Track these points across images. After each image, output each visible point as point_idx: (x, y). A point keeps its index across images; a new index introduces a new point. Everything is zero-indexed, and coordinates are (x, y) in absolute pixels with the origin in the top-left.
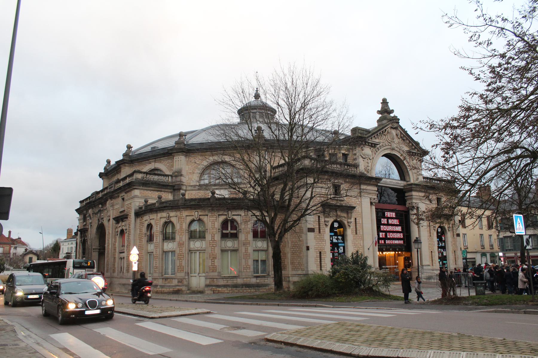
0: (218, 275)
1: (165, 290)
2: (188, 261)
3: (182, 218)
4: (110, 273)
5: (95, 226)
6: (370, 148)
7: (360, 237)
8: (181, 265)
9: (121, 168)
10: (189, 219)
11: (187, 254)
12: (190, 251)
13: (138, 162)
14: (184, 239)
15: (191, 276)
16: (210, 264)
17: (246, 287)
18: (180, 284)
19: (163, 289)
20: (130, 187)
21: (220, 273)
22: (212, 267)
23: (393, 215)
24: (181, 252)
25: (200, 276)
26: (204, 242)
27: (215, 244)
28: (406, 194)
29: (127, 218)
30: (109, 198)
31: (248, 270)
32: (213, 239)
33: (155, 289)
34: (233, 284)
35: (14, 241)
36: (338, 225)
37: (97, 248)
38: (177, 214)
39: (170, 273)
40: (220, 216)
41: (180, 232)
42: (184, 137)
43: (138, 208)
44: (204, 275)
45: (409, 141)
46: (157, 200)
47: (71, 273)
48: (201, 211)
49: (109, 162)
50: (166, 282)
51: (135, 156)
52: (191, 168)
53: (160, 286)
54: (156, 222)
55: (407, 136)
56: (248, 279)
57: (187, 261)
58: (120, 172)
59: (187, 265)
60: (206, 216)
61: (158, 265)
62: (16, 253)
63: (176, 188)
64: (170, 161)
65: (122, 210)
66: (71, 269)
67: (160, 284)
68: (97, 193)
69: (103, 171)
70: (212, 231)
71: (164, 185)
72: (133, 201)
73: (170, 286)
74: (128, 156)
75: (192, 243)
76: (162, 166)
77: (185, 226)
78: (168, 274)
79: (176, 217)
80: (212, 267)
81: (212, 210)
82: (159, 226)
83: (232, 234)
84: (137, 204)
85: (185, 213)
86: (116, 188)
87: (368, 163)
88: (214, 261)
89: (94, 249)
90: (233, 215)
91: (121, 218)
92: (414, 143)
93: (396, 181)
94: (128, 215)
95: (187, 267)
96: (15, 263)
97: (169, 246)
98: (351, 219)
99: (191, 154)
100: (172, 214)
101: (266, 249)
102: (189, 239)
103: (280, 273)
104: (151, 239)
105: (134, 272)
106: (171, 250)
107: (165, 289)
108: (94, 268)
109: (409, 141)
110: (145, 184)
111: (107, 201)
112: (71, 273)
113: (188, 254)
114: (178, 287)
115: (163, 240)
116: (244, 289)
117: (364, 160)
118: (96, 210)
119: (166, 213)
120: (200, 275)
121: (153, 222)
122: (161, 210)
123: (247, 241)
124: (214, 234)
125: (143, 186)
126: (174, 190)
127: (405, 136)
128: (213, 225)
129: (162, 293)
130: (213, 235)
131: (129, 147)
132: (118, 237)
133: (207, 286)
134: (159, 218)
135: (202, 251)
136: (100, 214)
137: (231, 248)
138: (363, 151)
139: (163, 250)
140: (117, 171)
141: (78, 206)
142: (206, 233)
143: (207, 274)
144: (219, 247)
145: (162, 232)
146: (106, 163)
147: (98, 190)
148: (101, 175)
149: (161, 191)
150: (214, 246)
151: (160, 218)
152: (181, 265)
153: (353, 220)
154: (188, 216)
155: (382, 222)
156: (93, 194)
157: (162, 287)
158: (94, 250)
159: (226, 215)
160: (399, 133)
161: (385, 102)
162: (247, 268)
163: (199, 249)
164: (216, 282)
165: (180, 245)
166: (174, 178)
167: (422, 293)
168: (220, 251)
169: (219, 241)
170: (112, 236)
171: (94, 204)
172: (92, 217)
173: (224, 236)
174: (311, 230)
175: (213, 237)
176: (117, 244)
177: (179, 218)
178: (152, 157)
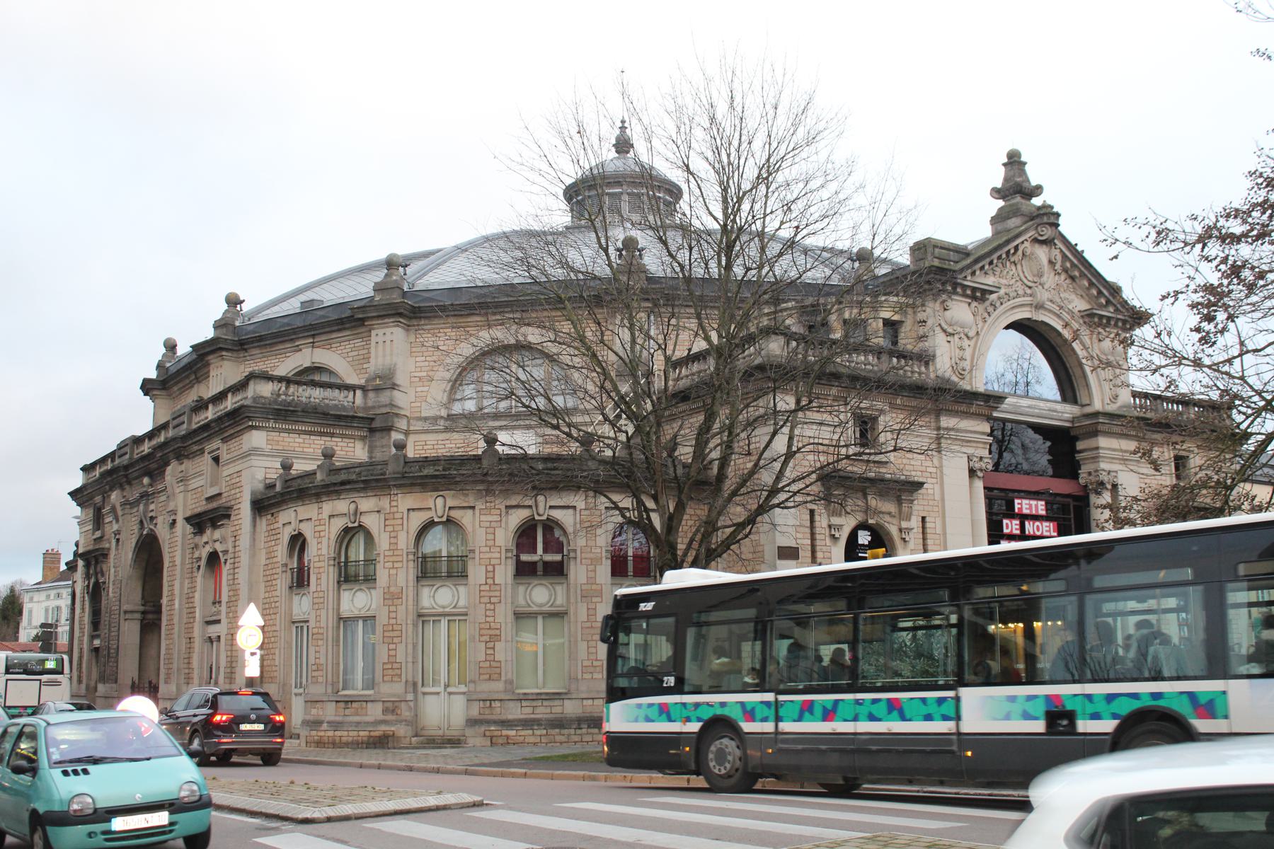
0: (505, 691)
1: (345, 735)
2: (415, 646)
5: (130, 543)
6: (969, 304)
8: (392, 660)
9: (208, 364)
10: (418, 520)
12: (420, 616)
14: (401, 581)
15: (424, 694)
17: (589, 727)
18: (390, 717)
20: (236, 424)
21: (511, 682)
22: (487, 664)
24: (393, 621)
25: (450, 694)
26: (462, 589)
27: (498, 594)
29: (228, 517)
31: (596, 676)
32: (490, 581)
33: (314, 733)
36: (869, 538)
37: (136, 608)
39: (360, 685)
40: (511, 511)
41: (391, 559)
42: (401, 269)
43: (261, 486)
44: (463, 688)
45: (1089, 281)
46: (319, 463)
49: (171, 346)
50: (347, 712)
52: (423, 364)
53: (328, 722)
57: (410, 647)
59: (410, 659)
60: (470, 512)
61: (323, 661)
64: (358, 342)
65: (212, 491)
67: (328, 718)
74: (231, 328)
75: (346, 596)
77: (405, 541)
80: (487, 664)
81: (489, 492)
82: (325, 541)
83: (546, 564)
84: (260, 475)
85: (405, 501)
87: (961, 348)
88: (494, 648)
89: (126, 612)
92: (1105, 287)
93: (1049, 405)
95: (410, 665)
98: (908, 519)
99: (423, 322)
100: (366, 504)
104: (301, 580)
106: (363, 613)
107: (346, 733)
109: (1089, 281)
110: (284, 414)
111: (167, 464)
113: (415, 625)
114: (383, 728)
115: (339, 582)
116: (584, 731)
117: (949, 339)
118: (133, 494)
119: (348, 501)
120: (449, 690)
121: (307, 530)
122: (336, 492)
123: (594, 587)
124: (494, 566)
126: (372, 431)
127: (1076, 266)
128: (491, 537)
129: (335, 744)
130: (490, 568)
134: (325, 515)
135: (456, 616)
136: (146, 505)
137: (546, 609)
140: (195, 373)
141: (78, 481)
143: (472, 685)
144: (509, 606)
148: (148, 387)
150: (493, 600)
152: (392, 660)
153: (915, 523)
154: (413, 510)
155: (1006, 531)
156: (122, 446)
157: (336, 725)
159: (530, 507)
160: (1059, 258)
161: (1014, 162)
162: (592, 669)
163: (447, 610)
165: (392, 597)
166: (371, 395)
168: (510, 617)
169: (509, 587)
171: (126, 476)
172: (120, 513)
173: (524, 571)
175: (491, 574)
176: (197, 595)
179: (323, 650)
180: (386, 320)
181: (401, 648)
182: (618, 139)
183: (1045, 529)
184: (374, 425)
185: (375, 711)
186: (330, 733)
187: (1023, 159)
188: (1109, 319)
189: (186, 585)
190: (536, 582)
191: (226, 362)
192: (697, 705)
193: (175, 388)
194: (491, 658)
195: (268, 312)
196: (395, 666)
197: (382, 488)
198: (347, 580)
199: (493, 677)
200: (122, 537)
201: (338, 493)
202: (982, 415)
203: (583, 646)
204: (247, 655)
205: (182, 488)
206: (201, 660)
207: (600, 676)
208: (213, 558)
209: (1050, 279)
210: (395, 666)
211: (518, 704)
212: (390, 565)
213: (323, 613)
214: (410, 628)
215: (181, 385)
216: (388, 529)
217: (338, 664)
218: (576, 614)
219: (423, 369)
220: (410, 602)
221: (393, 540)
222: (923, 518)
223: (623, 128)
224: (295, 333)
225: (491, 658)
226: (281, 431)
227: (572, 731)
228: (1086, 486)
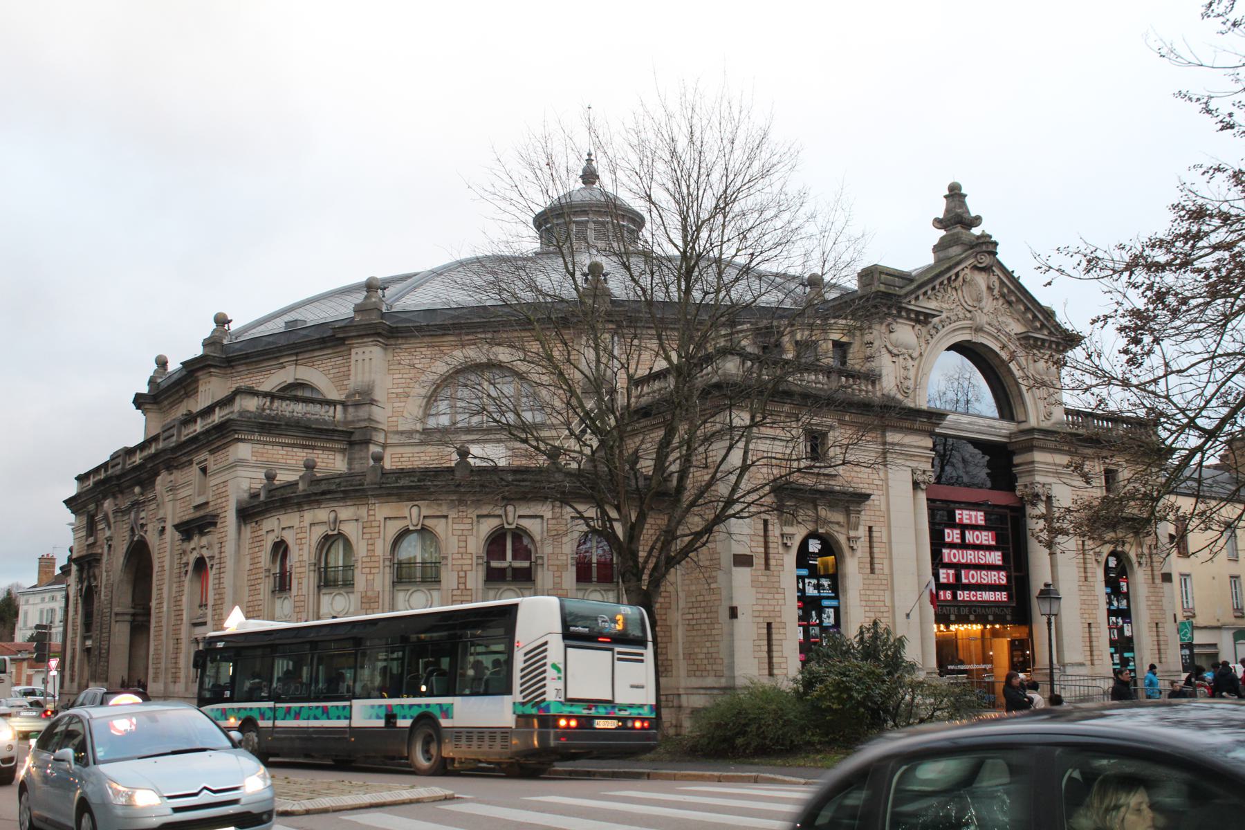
3: (374, 524)
4: (166, 684)
5: (121, 548)
6: (913, 327)
7: (884, 582)
9: (197, 381)
10: (393, 528)
13: (245, 364)
14: (378, 585)
20: (223, 436)
28: (1017, 459)
29: (215, 524)
36: (819, 547)
38: (359, 512)
40: (482, 520)
43: (246, 496)
46: (301, 474)
47: (555, 666)
48: (428, 506)
49: (162, 363)
51: (237, 346)
55: (1020, 291)
58: (196, 391)
63: (356, 437)
64: (339, 360)
66: (556, 645)
68: (129, 452)
70: (460, 562)
71: (320, 431)
72: (234, 475)
74: (219, 346)
77: (382, 548)
81: (461, 502)
83: (515, 570)
84: (245, 485)
85: (382, 510)
87: (906, 368)
89: (117, 614)
90: (520, 517)
92: (1039, 311)
94: (217, 516)
98: (856, 528)
99: (400, 342)
100: (345, 513)
110: (268, 427)
111: (158, 474)
112: (555, 666)
115: (319, 587)
117: (894, 359)
118: (125, 502)
119: (328, 510)
121: (289, 537)
124: (465, 572)
125: (261, 434)
126: (352, 444)
127: (1013, 292)
128: (463, 544)
130: (462, 574)
131: (221, 321)
134: (306, 523)
136: (137, 513)
138: (893, 335)
141: (72, 490)
142: (443, 569)
145: (317, 563)
147: (132, 444)
148: (139, 401)
149: (314, 448)
151: (312, 524)
153: (862, 532)
154: (390, 518)
155: (947, 540)
156: (114, 457)
158: (119, 618)
159: (500, 516)
160: (997, 284)
166: (351, 410)
171: (118, 485)
172: (112, 520)
174: (743, 561)
175: (462, 580)
176: (184, 599)
180: (365, 340)
182: (584, 171)
184: (353, 439)
187: (963, 191)
188: (1043, 341)
189: (174, 589)
190: (506, 587)
191: (213, 378)
192: (411, 706)
202: (925, 431)
209: (988, 304)
216: (365, 536)
219: (400, 385)
221: (370, 547)
222: (870, 528)
226: (265, 443)
228: (1022, 498)
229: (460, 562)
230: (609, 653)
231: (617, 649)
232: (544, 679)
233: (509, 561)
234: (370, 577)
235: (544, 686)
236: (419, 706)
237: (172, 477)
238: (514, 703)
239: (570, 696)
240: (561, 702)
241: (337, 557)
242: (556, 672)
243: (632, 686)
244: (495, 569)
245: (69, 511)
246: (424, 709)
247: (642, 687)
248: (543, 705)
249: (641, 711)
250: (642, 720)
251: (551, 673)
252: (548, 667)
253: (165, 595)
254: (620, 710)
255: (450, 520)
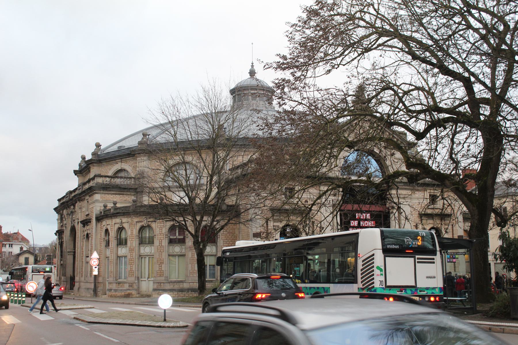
0: (165, 280)
1: (118, 294)
2: (138, 265)
4: (79, 277)
5: (69, 228)
8: (131, 270)
9: (90, 168)
10: (139, 225)
11: (137, 259)
12: (140, 256)
13: (106, 162)
14: (134, 245)
15: (141, 281)
16: (158, 269)
17: (191, 292)
18: (131, 288)
19: (116, 293)
20: (91, 192)
21: (167, 277)
22: (159, 271)
23: (368, 216)
24: (132, 258)
25: (149, 281)
26: (153, 247)
27: (163, 249)
29: (90, 222)
30: (77, 200)
31: (194, 275)
33: (110, 293)
34: (179, 288)
35: (9, 237)
37: (71, 251)
39: (123, 277)
42: (147, 136)
43: (99, 212)
44: (153, 279)
45: (389, 132)
47: (378, 268)
49: (83, 158)
50: (119, 286)
51: (103, 155)
54: (112, 227)
56: (194, 284)
57: (137, 266)
58: (89, 171)
59: (137, 270)
61: (112, 270)
62: (12, 252)
64: (134, 161)
65: (87, 213)
66: (379, 256)
68: (71, 192)
69: (77, 168)
70: (160, 237)
71: (125, 189)
72: (94, 205)
73: (122, 290)
74: (97, 155)
75: (142, 248)
76: (127, 165)
77: (135, 232)
78: (122, 279)
79: (127, 223)
80: (159, 271)
83: (179, 239)
84: (98, 209)
86: (84, 190)
88: (161, 266)
89: (68, 252)
91: (86, 223)
94: (91, 219)
95: (137, 272)
96: (7, 265)
97: (122, 251)
100: (125, 220)
101: (215, 254)
102: (139, 244)
103: (203, 278)
104: (108, 244)
105: (95, 276)
106: (124, 255)
107: (118, 293)
108: (435, 254)
110: (105, 188)
111: (76, 202)
112: (378, 268)
113: (138, 259)
114: (129, 291)
115: (117, 245)
116: (190, 293)
118: (69, 211)
119: (119, 219)
121: (109, 227)
122: (115, 216)
125: (103, 190)
128: (161, 231)
129: (116, 297)
130: (161, 241)
131: (98, 145)
132: (85, 240)
133: (154, 290)
134: (113, 223)
135: (151, 256)
136: (72, 216)
137: (179, 253)
139: (117, 255)
141: (57, 204)
142: (154, 239)
143: (155, 278)
144: (166, 253)
145: (117, 237)
146: (81, 159)
147: (72, 189)
148: (76, 172)
150: (161, 251)
151: (115, 224)
152: (131, 270)
155: (351, 225)
156: (67, 194)
157: (116, 290)
158: (69, 253)
162: (193, 273)
163: (148, 254)
164: (163, 286)
165: (131, 250)
167: (360, 298)
168: (167, 256)
169: (167, 247)
170: (80, 239)
171: (67, 205)
172: (66, 218)
173: (171, 242)
175: (161, 243)
176: (84, 247)
177: (131, 224)
178: (118, 157)
179: (113, 266)
181: (134, 266)
182: (250, 71)
183: (369, 224)
185: (126, 286)
186: (114, 293)
189: (82, 244)
190: (176, 245)
191: (95, 167)
192: (310, 288)
193: (84, 173)
194: (160, 269)
195: (112, 148)
196: (132, 272)
197: (128, 215)
198: (120, 244)
199: (161, 275)
200: (67, 226)
201: (116, 216)
203: (190, 266)
204: (94, 267)
205: (80, 211)
206: (85, 270)
207: (196, 275)
208: (88, 234)
210: (132, 272)
211: (169, 284)
212: (131, 240)
213: (113, 255)
214: (137, 260)
215: (85, 172)
217: (117, 271)
218: (188, 255)
220: (137, 252)
221: (132, 232)
223: (252, 66)
224: (115, 158)
225: (160, 269)
226: (105, 194)
227: (186, 293)
229: (160, 237)
230: (413, 259)
231: (417, 257)
232: (373, 275)
233: (177, 236)
234: (132, 242)
235: (373, 279)
236: (314, 288)
237: (80, 204)
238: (358, 288)
239: (388, 284)
240: (383, 288)
241: (123, 236)
242: (379, 271)
243: (427, 277)
244: (172, 239)
245: (55, 212)
246: (316, 290)
247: (434, 277)
248: (373, 290)
249: (434, 291)
250: (435, 296)
251: (377, 272)
252: (375, 268)
253: (79, 246)
254: (420, 291)
255: (157, 223)
